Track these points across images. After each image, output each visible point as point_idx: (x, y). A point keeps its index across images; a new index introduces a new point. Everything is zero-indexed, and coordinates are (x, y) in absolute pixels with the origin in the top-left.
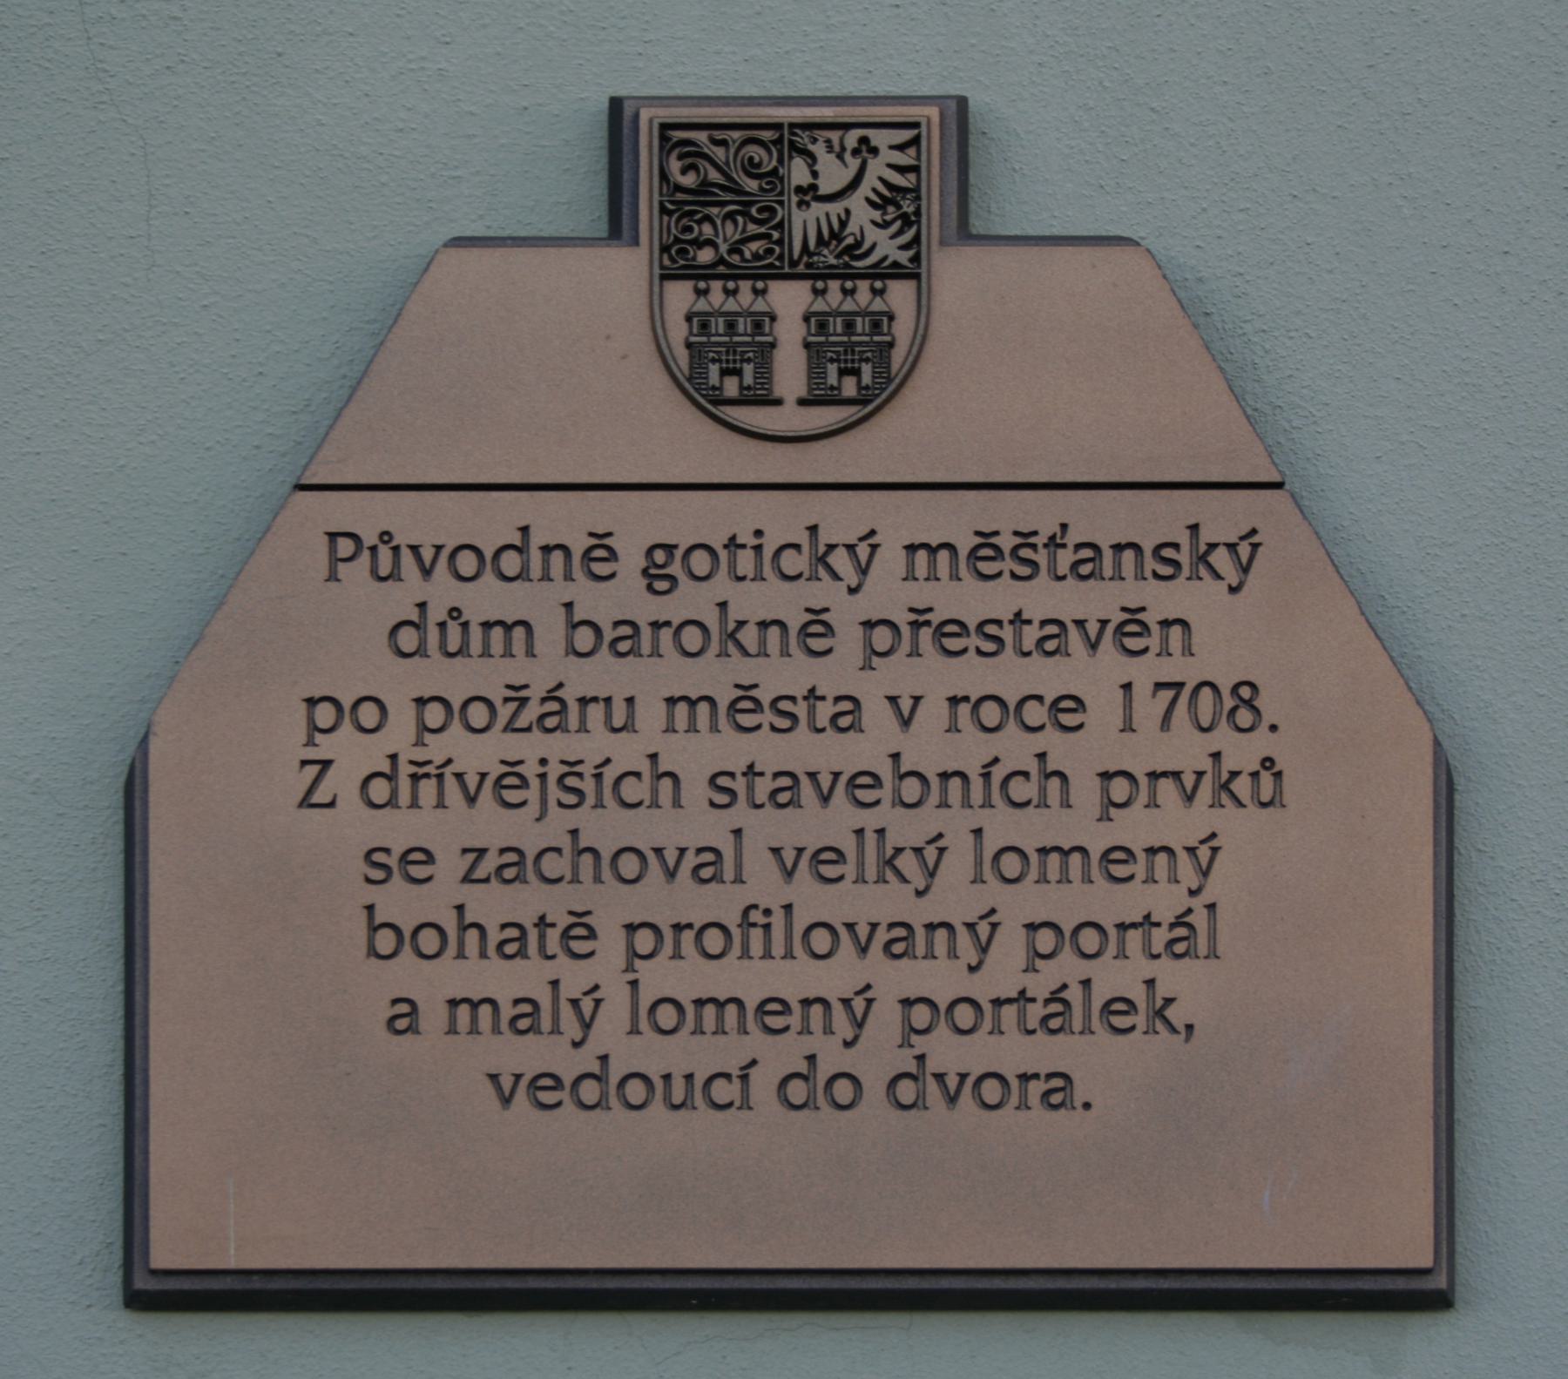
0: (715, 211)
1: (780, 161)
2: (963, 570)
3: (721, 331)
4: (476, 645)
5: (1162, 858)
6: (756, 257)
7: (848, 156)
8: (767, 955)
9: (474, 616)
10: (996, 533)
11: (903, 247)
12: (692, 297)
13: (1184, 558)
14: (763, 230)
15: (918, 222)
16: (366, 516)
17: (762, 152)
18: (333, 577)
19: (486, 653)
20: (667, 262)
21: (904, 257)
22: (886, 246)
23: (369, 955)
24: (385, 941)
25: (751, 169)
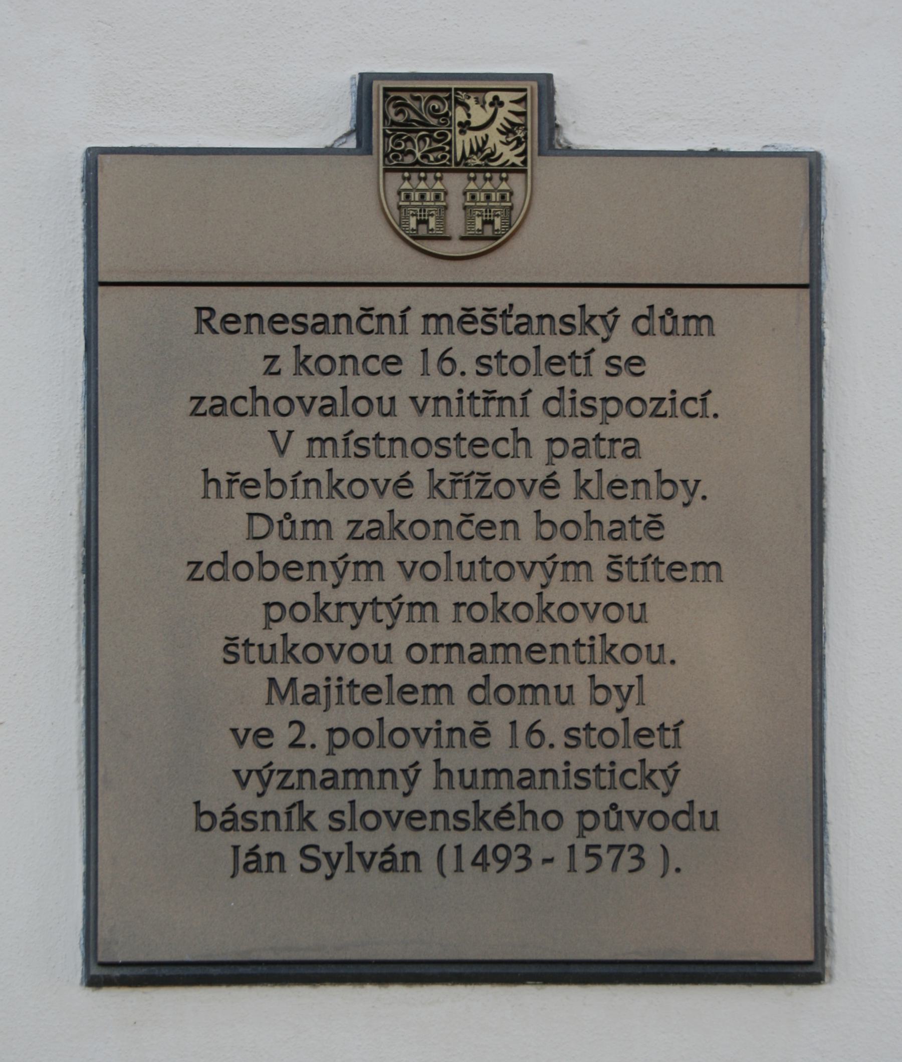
0: (412, 135)
1: (450, 108)
2: (266, 329)
3: (417, 199)
5: (642, 486)
6: (437, 160)
7: (487, 106)
10: (474, 309)
11: (518, 155)
12: (466, 181)
13: (577, 322)
14: (440, 145)
15: (526, 142)
17: (440, 104)
20: (387, 162)
21: (518, 161)
22: (509, 155)
25: (434, 113)
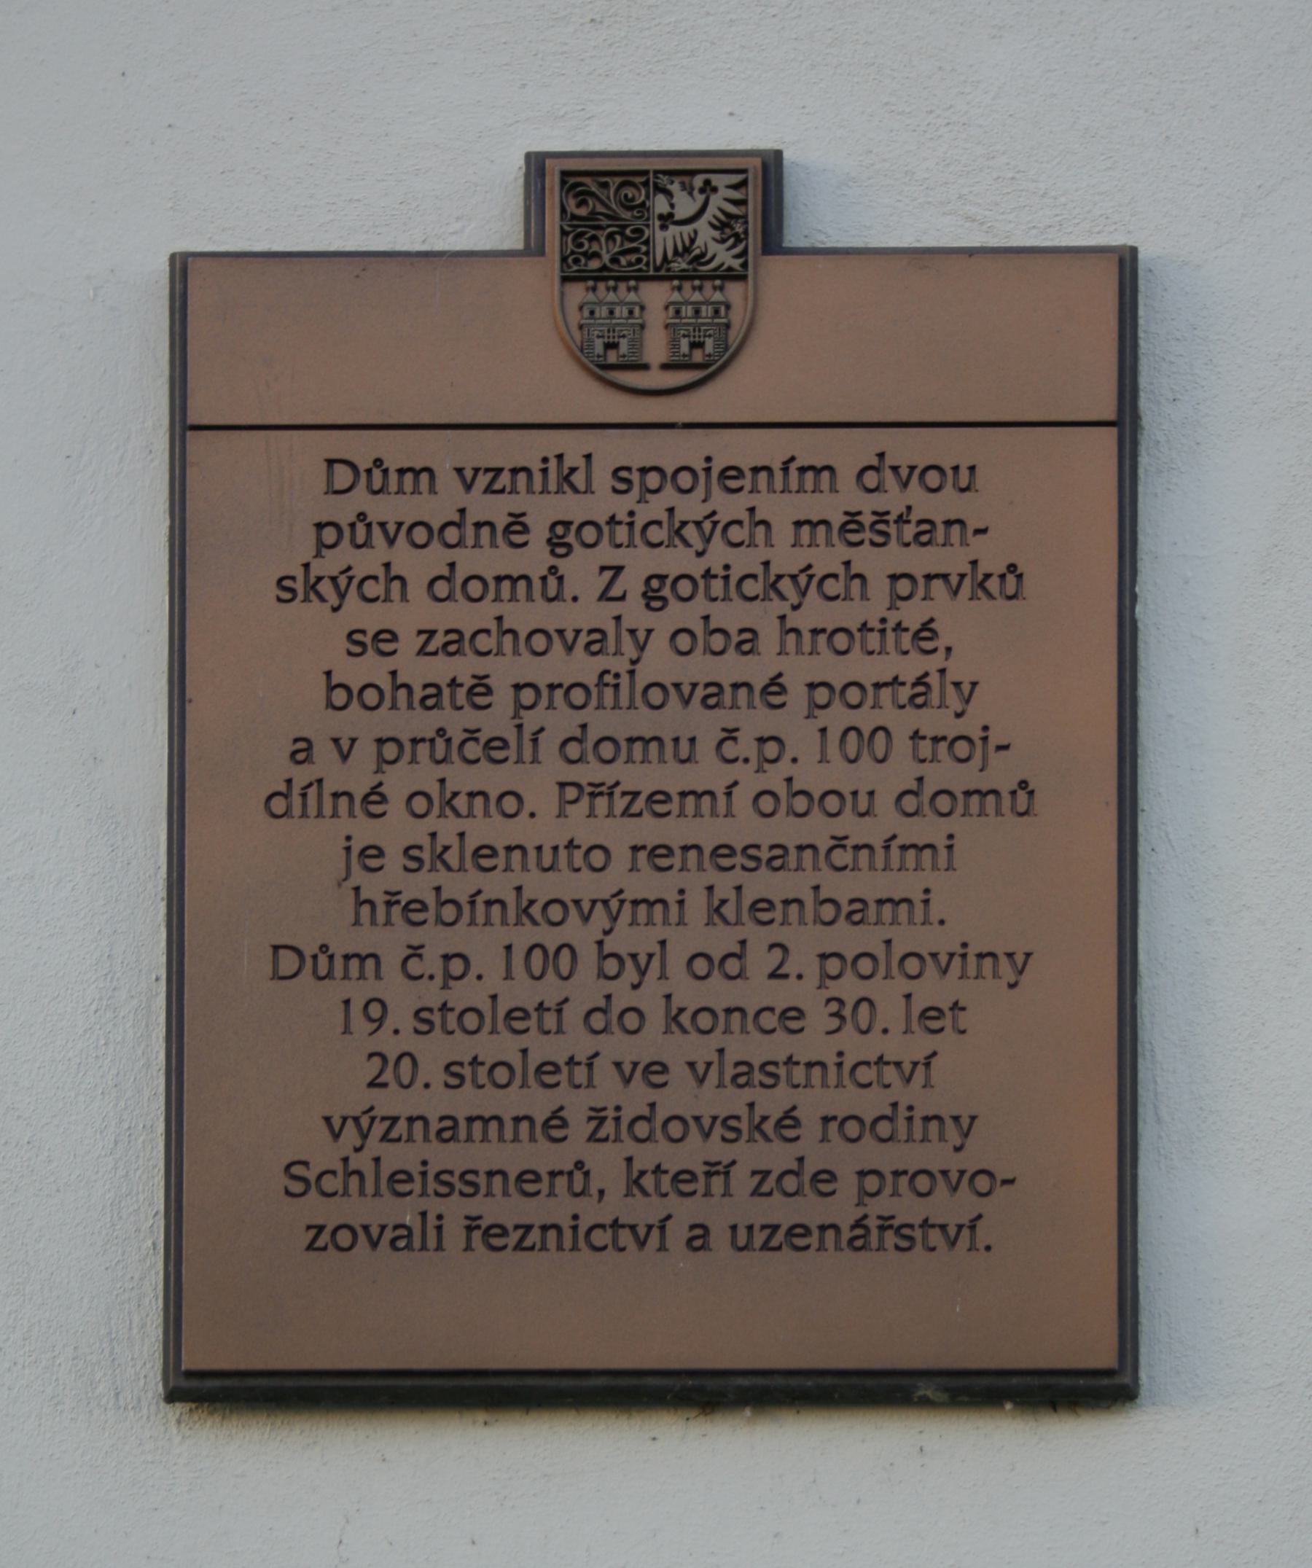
1: (648, 197)
4: (393, 485)
6: (630, 264)
7: (696, 193)
8: (616, 706)
9: (392, 464)
11: (737, 256)
14: (634, 245)
15: (746, 238)
16: (361, 448)
18: (561, 814)
19: (400, 491)
21: (736, 263)
22: (724, 256)
23: (327, 707)
24: (339, 697)
25: (628, 204)
